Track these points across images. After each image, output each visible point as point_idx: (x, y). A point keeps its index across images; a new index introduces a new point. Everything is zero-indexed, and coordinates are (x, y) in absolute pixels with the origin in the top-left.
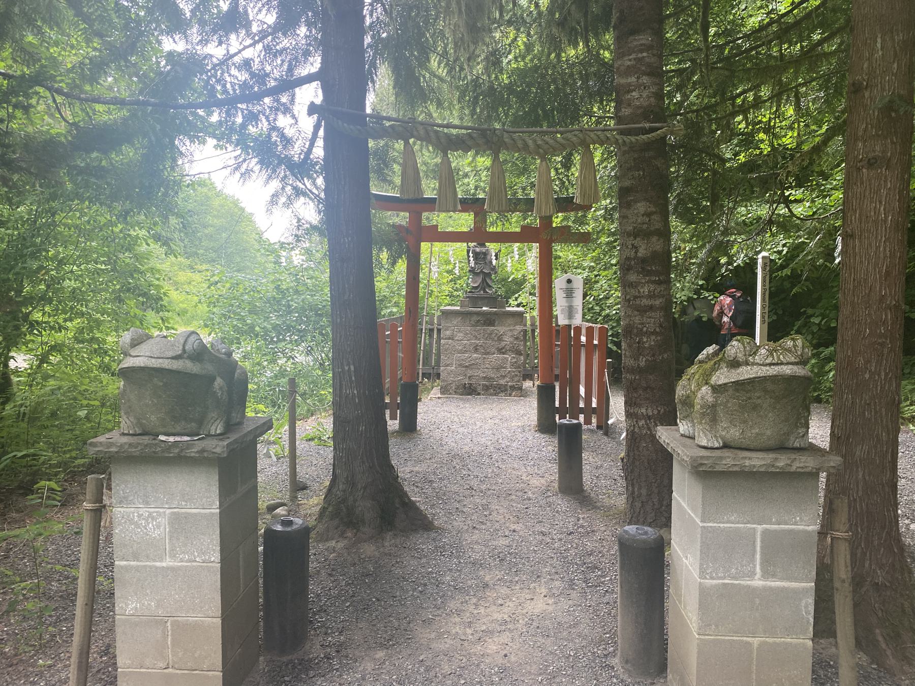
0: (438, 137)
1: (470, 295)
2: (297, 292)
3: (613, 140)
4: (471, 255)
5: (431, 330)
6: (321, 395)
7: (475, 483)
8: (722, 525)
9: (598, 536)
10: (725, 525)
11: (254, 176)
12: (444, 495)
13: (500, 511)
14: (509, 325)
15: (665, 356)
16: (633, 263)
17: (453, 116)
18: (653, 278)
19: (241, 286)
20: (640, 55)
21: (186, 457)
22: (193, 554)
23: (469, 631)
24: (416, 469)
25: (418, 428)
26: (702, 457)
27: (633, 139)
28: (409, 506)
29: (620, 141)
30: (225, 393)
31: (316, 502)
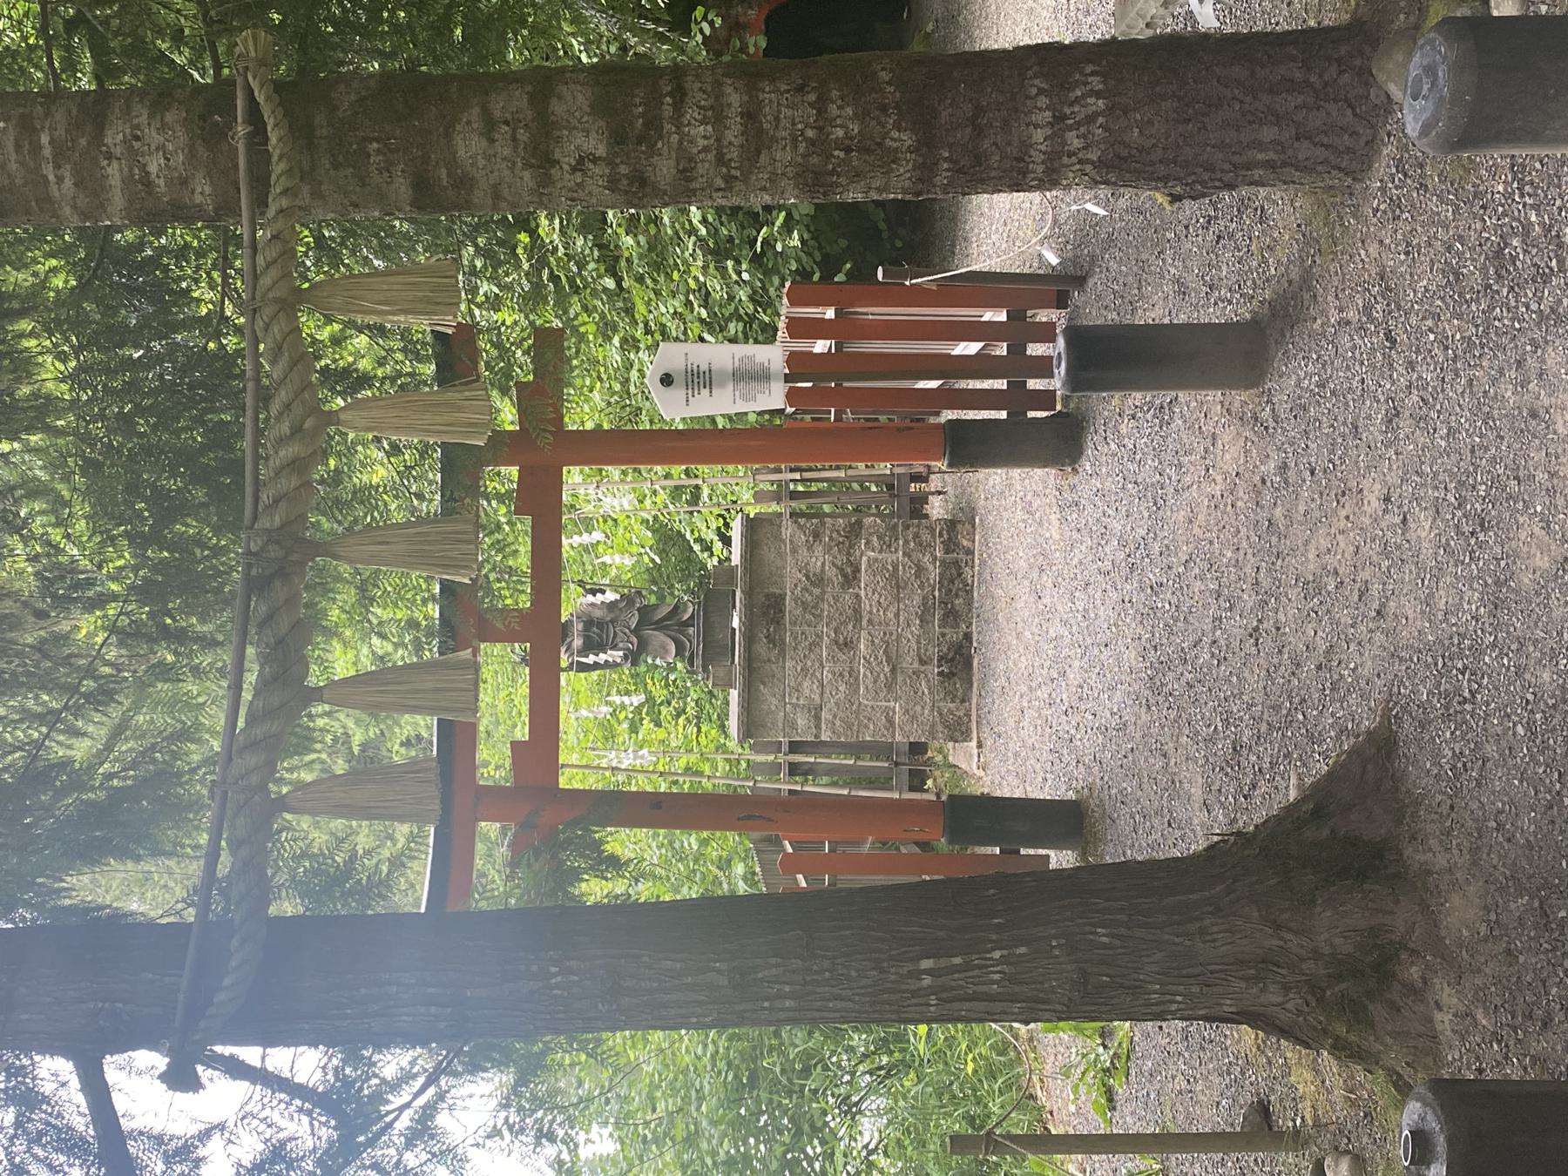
0: (268, 714)
1: (698, 662)
2: (691, 1140)
3: (280, 225)
4: (591, 659)
5: (794, 770)
6: (975, 1071)
7: (1236, 625)
12: (1276, 708)
13: (1326, 546)
14: (781, 555)
16: (624, 169)
17: (209, 700)
18: (667, 111)
20: (47, 152)
24: (1197, 792)
25: (1071, 795)
27: (278, 168)
28: (1319, 802)
29: (284, 203)
31: (1308, 1076)
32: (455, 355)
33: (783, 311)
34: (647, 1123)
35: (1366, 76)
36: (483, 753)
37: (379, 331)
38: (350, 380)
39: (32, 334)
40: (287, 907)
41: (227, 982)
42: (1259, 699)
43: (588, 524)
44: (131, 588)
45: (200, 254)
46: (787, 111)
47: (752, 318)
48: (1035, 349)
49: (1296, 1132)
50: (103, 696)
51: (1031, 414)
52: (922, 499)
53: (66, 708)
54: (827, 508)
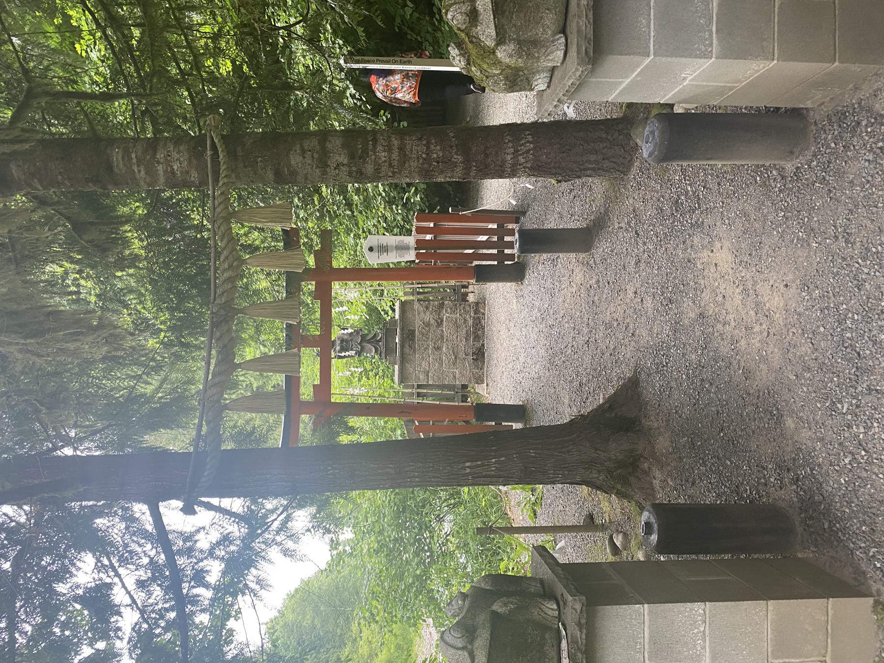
2: (381, 532)
3: (224, 189)
4: (343, 354)
5: (419, 395)
7: (581, 340)
8: (652, 34)
9: (639, 205)
10: (652, 29)
11: (263, 575)
12: (595, 370)
13: (613, 310)
14: (414, 316)
15: (451, 134)
16: (354, 169)
17: (199, 369)
18: (371, 147)
19: (375, 590)
20: (134, 160)
21: (586, 645)
22: (696, 635)
23: (757, 329)
24: (566, 401)
25: (521, 403)
26: (578, 52)
27: (223, 167)
28: (612, 403)
30: (511, 599)
31: (607, 504)
32: (290, 238)
33: (414, 224)
34: (365, 526)
35: (629, 137)
36: (303, 390)
37: (261, 230)
38: (252, 249)
39: (130, 231)
40: (229, 446)
41: (205, 474)
42: (589, 366)
43: (341, 304)
44: (169, 327)
45: (194, 202)
46: (415, 147)
47: (403, 227)
48: (507, 239)
49: (603, 525)
50: (158, 368)
51: (506, 263)
52: (466, 294)
53: (143, 373)
54: (431, 298)
